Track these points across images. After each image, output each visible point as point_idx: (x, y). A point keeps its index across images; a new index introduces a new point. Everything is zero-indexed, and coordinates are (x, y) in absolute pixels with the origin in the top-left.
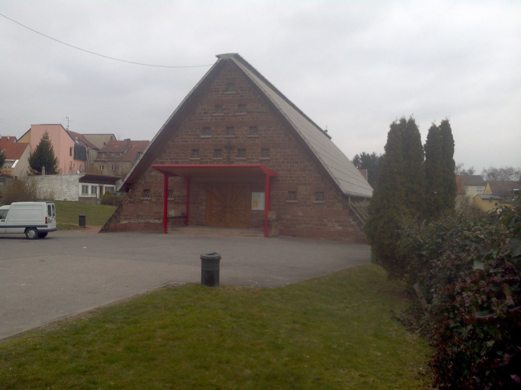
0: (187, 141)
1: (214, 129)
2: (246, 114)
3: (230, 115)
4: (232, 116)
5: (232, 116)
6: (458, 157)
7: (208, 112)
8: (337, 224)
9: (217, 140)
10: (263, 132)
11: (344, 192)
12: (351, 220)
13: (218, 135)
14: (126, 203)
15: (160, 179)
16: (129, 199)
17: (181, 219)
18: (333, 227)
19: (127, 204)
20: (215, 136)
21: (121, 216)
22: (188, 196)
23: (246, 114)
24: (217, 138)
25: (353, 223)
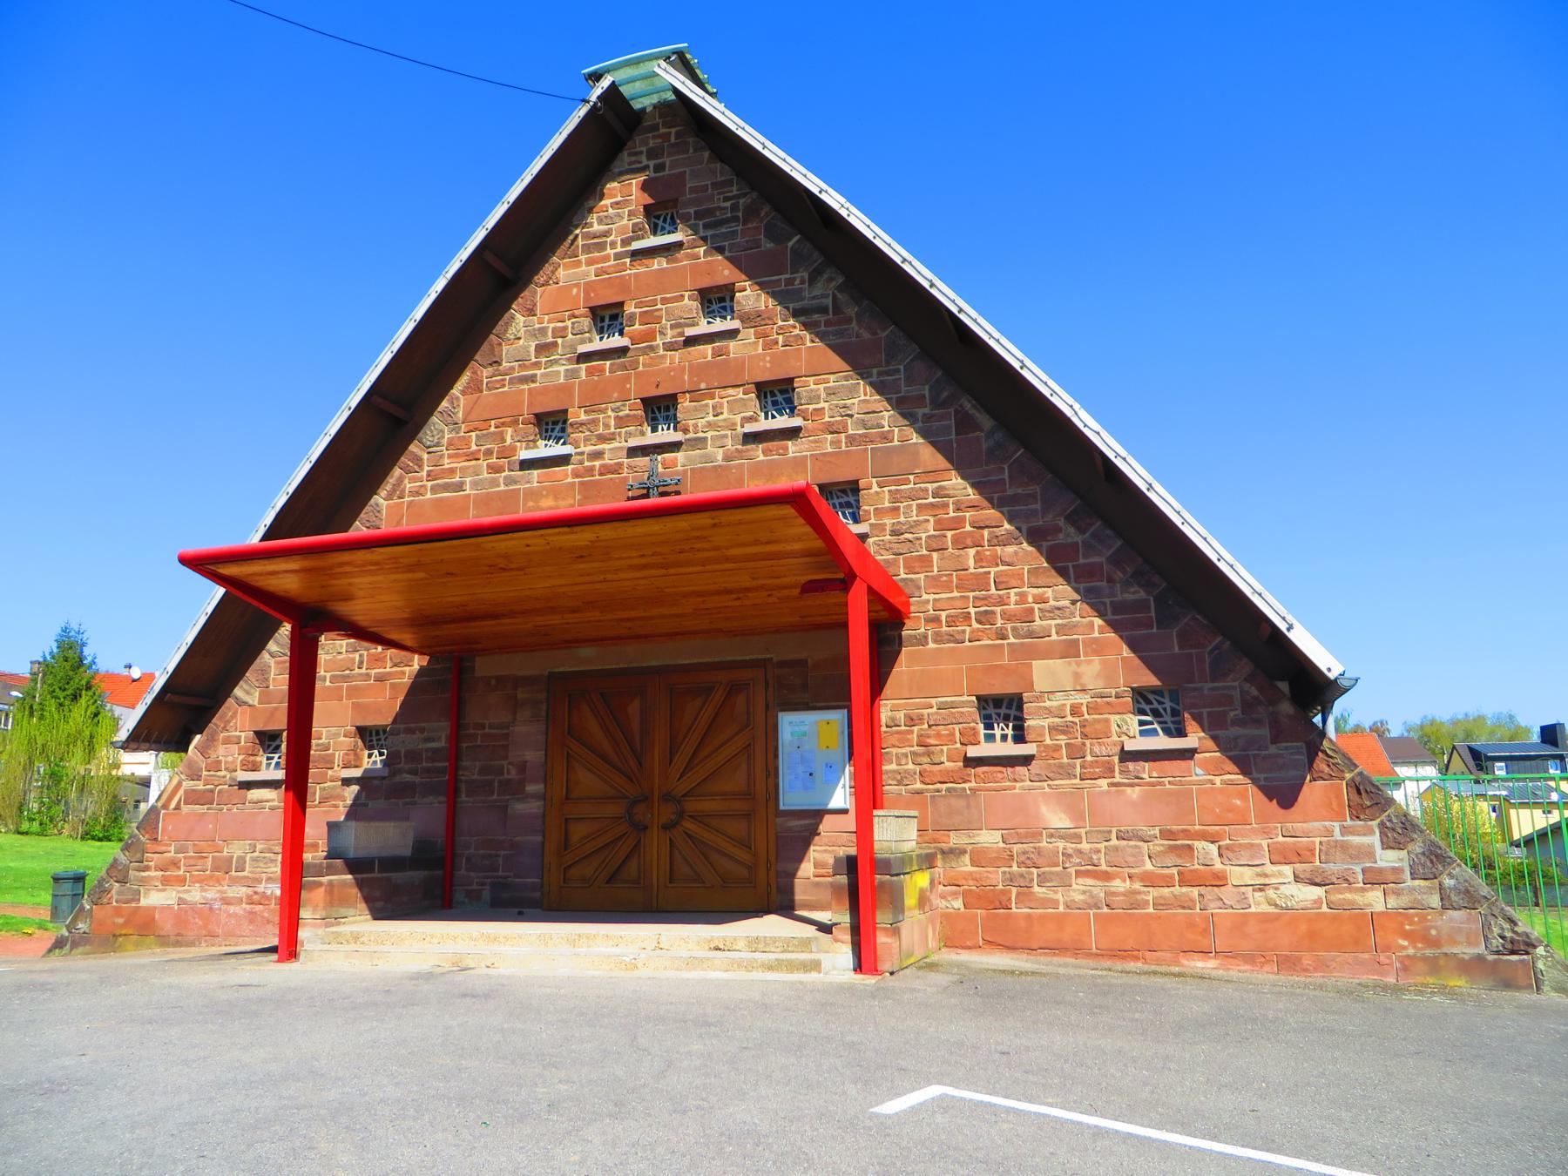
0: (460, 487)
1: (583, 417)
2: (1410, 988)
3: (659, 341)
4: (670, 347)
5: (670, 347)
6: (877, 846)
7: (560, 341)
8: (1287, 870)
9: (597, 463)
10: (822, 405)
11: (1324, 669)
12: (1375, 840)
13: (603, 439)
14: (173, 804)
15: (328, 675)
16: (187, 784)
17: (398, 877)
18: (1262, 888)
19: (178, 808)
20: (589, 448)
21: (147, 868)
22: (454, 754)
23: (1410, 988)
24: (597, 455)
25: (1388, 859)
